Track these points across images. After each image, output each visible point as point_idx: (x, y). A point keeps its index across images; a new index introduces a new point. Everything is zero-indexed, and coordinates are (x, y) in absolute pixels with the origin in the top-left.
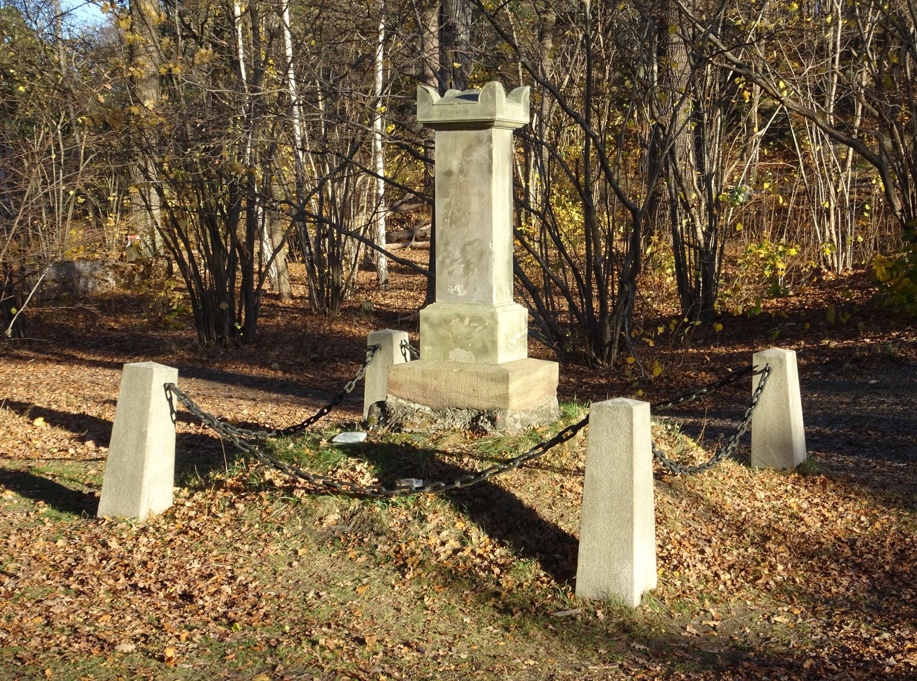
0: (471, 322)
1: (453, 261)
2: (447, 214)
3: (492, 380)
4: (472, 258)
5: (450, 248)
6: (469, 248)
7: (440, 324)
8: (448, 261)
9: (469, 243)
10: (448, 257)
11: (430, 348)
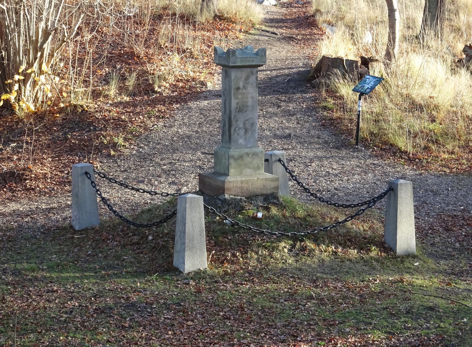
0: (252, 156)
1: (240, 128)
2: (237, 107)
3: (272, 181)
4: (248, 126)
5: (238, 123)
6: (247, 122)
7: (238, 159)
8: (237, 129)
9: (247, 120)
10: (237, 127)
11: (234, 170)
